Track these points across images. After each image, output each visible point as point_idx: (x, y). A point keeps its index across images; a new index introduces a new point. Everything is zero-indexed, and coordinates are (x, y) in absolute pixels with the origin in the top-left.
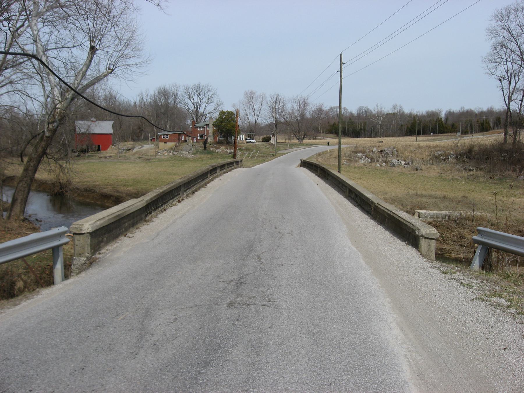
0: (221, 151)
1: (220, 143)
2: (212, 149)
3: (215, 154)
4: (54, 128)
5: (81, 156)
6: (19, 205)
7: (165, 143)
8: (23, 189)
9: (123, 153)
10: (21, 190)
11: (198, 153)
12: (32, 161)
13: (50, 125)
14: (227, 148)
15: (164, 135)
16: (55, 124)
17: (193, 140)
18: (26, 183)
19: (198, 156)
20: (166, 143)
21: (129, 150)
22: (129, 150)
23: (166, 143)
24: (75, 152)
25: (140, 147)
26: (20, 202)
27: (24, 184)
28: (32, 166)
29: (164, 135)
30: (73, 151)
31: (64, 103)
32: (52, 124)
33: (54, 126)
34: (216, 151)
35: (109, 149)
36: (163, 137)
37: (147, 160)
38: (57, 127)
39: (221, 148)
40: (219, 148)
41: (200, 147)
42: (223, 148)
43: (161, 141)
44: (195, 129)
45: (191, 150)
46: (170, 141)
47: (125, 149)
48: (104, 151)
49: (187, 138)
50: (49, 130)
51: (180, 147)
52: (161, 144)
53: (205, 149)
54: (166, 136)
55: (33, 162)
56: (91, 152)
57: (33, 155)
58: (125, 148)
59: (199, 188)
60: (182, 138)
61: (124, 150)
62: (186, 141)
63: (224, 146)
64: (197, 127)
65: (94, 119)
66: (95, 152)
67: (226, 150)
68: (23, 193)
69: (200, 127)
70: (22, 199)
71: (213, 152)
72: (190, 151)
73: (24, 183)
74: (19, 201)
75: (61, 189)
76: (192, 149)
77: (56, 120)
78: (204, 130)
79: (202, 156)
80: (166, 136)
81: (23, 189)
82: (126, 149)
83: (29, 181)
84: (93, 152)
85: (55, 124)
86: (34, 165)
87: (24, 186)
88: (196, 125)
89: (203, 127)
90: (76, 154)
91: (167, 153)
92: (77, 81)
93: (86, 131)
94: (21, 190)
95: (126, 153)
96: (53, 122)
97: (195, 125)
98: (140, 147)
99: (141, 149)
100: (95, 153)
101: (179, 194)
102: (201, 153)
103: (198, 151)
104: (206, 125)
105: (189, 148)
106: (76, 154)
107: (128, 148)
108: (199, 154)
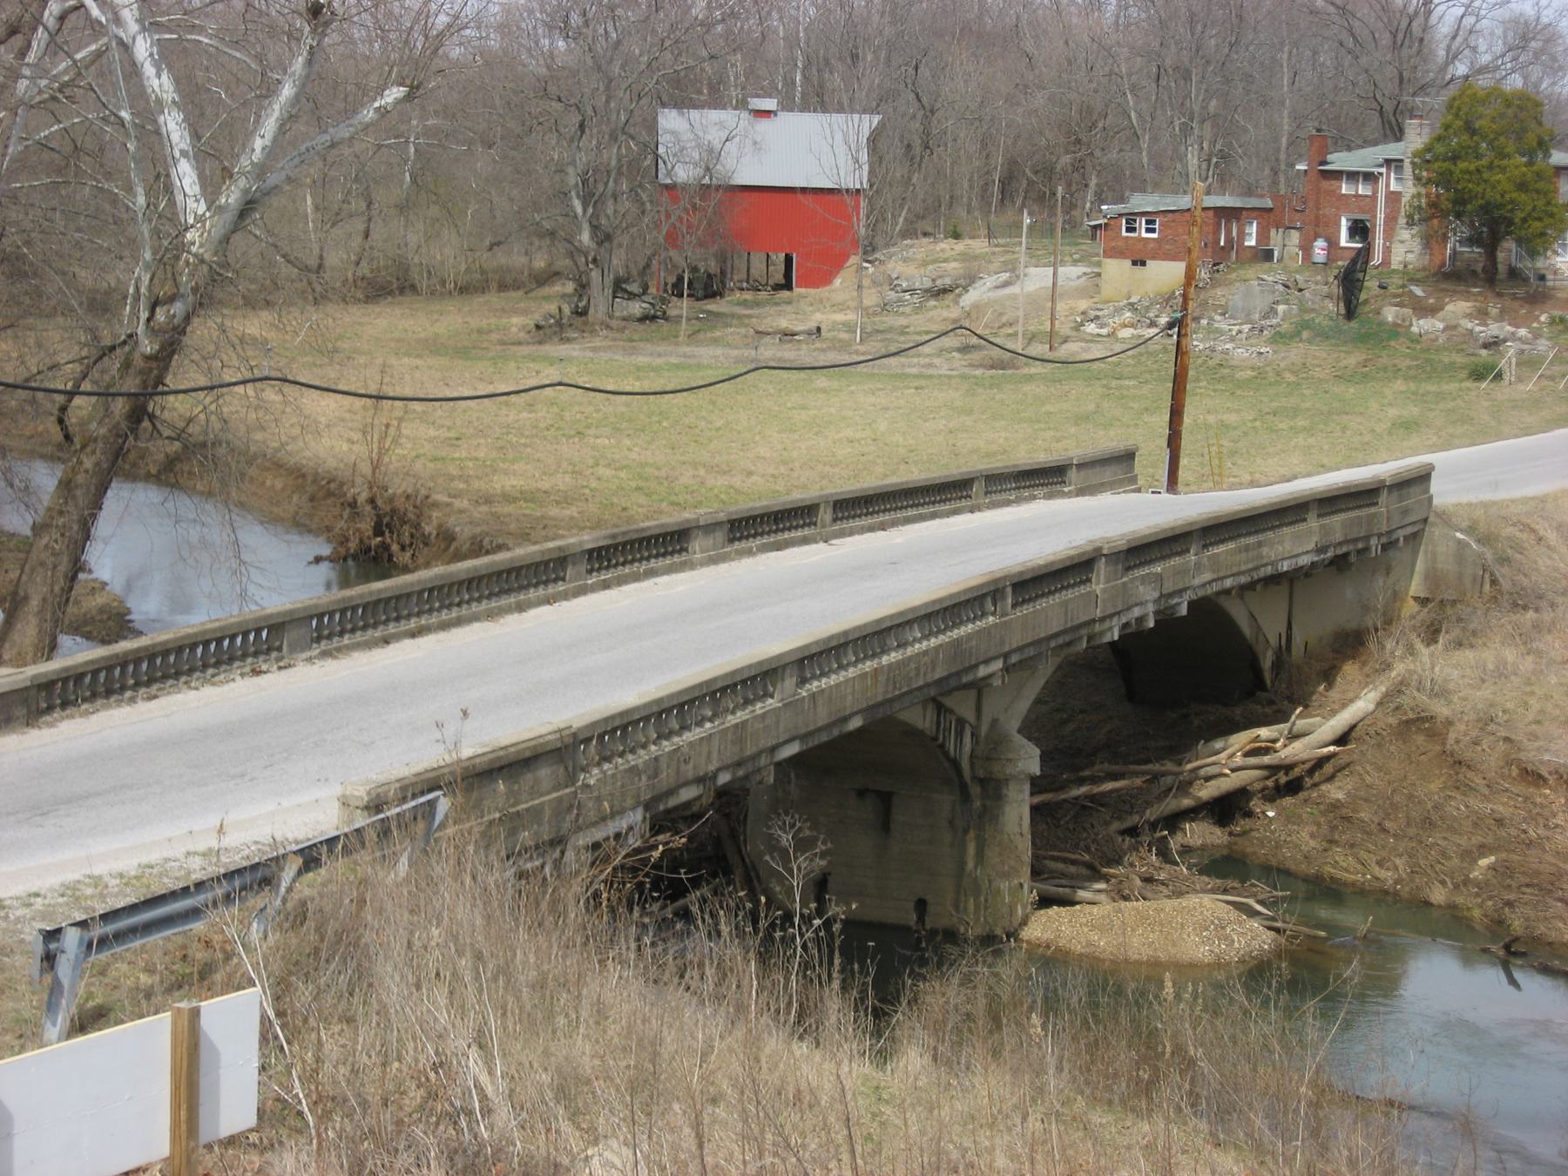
0: (1441, 326)
1: (1452, 277)
2: (1390, 314)
3: (1400, 346)
4: (176, 321)
5: (665, 317)
6: (33, 621)
7: (1134, 263)
8: (50, 561)
9: (908, 310)
10: (42, 564)
11: (1305, 334)
12: (89, 449)
13: (158, 310)
14: (1482, 315)
15: (1131, 219)
16: (178, 308)
17: (1306, 248)
18: (63, 535)
19: (1295, 353)
20: (1143, 263)
21: (940, 293)
22: (940, 293)
23: (1143, 263)
24: (632, 296)
25: (1005, 276)
26: (36, 609)
27: (56, 541)
28: (86, 471)
29: (1131, 219)
30: (619, 287)
31: (212, 226)
32: (165, 308)
33: (174, 316)
34: (1415, 329)
35: (837, 282)
36: (1129, 230)
37: (992, 367)
38: (187, 319)
39: (1450, 307)
40: (1432, 311)
41: (1329, 296)
42: (1458, 308)
43: (1112, 253)
44: (1325, 184)
45: (1272, 312)
46: (1161, 252)
47: (917, 285)
48: (812, 291)
49: (1276, 237)
50: (152, 331)
51: (1219, 292)
52: (1116, 270)
53: (1350, 314)
54: (1142, 224)
55: (94, 452)
56: (738, 295)
57: (94, 425)
58: (921, 278)
59: (475, 618)
60: (1242, 235)
61: (911, 291)
62: (1268, 256)
63: (1467, 296)
64: (1337, 175)
65: (770, 104)
66: (763, 295)
67: (1469, 326)
68: (49, 573)
69: (1352, 176)
70: (44, 600)
71: (1397, 331)
72: (1265, 317)
73: (55, 535)
74: (34, 603)
75: (378, 531)
76: (1281, 308)
77: (182, 290)
78: (1375, 192)
79: (1319, 353)
80: (1142, 224)
81: (50, 561)
82: (928, 284)
83: (75, 527)
84: (748, 296)
85: (178, 308)
86: (97, 464)
87: (57, 547)
88: (1330, 157)
89: (1370, 177)
90: (637, 308)
91: (1132, 326)
92: (263, 137)
93: (700, 171)
94: (42, 564)
95: (919, 309)
96: (171, 299)
97: (1325, 163)
98: (1005, 276)
99: (1014, 290)
100: (757, 304)
101: (279, 649)
102: (1322, 335)
103: (1305, 325)
104: (1388, 162)
105: (1260, 303)
106: (637, 308)
107: (939, 282)
108: (1310, 342)
